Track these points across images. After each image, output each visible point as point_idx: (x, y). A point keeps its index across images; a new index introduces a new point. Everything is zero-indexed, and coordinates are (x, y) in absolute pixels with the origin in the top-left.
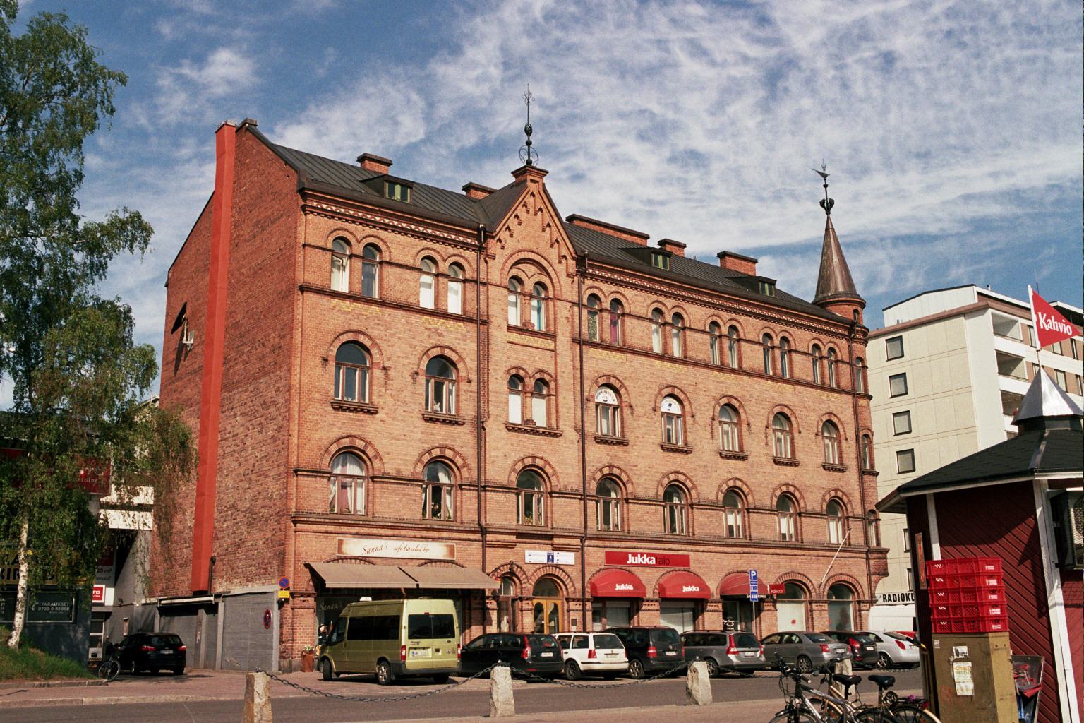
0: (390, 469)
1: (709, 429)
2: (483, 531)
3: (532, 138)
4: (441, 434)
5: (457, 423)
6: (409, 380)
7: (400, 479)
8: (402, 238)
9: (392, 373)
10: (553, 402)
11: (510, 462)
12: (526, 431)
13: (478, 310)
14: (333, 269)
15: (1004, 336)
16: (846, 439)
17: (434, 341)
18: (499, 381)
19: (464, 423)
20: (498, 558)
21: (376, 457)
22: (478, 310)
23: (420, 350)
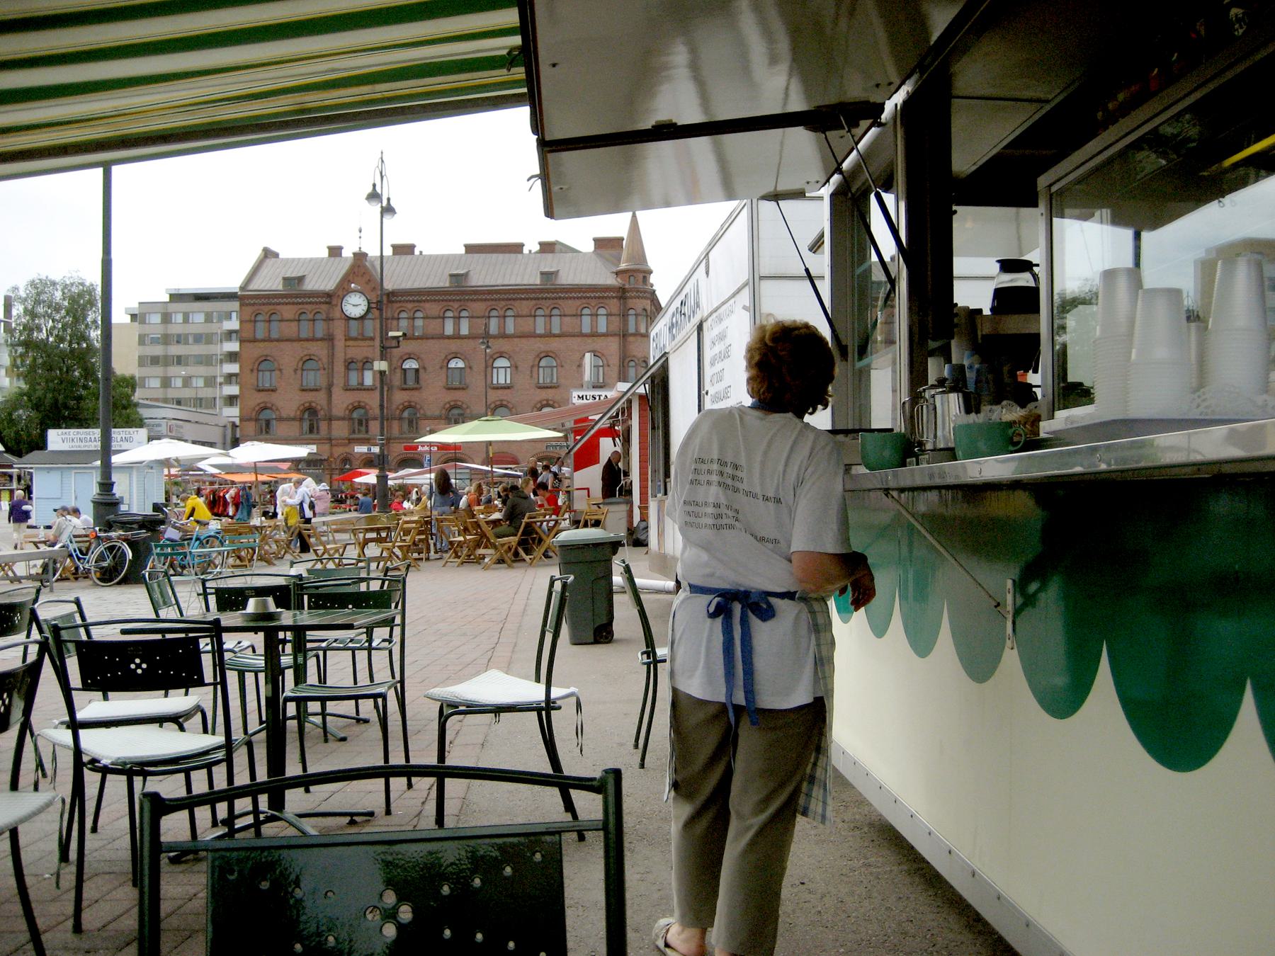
0: (284, 415)
1: (483, 374)
2: (330, 439)
3: (362, 234)
4: (309, 397)
5: (317, 390)
6: (293, 373)
7: (289, 419)
8: (289, 307)
9: (284, 371)
10: (489, 382)
11: (345, 405)
12: (361, 390)
13: (264, 321)
14: (900, 427)
15: (609, 642)
16: (609, 366)
17: (305, 353)
18: (339, 367)
19: (320, 389)
20: (339, 451)
21: (554, 402)
22: (264, 321)
23: (298, 358)
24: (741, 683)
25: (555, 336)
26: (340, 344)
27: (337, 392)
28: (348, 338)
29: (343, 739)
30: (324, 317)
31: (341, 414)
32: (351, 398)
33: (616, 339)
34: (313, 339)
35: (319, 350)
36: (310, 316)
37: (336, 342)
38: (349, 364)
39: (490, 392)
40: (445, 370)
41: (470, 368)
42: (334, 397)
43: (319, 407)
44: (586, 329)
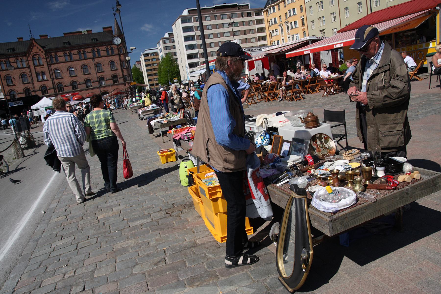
4: (26, 85)
18: (34, 75)
24: (109, 175)
25: (68, 62)
26: (32, 68)
27: (36, 83)
28: (35, 66)
29: (281, 122)
30: (25, 60)
31: (38, 89)
32: (40, 84)
33: (118, 56)
34: (23, 68)
35: (26, 71)
36: (20, 60)
37: (31, 68)
38: (37, 74)
39: (98, 74)
40: (68, 71)
41: (76, 70)
42: (35, 84)
43: (30, 88)
44: (20, 66)
